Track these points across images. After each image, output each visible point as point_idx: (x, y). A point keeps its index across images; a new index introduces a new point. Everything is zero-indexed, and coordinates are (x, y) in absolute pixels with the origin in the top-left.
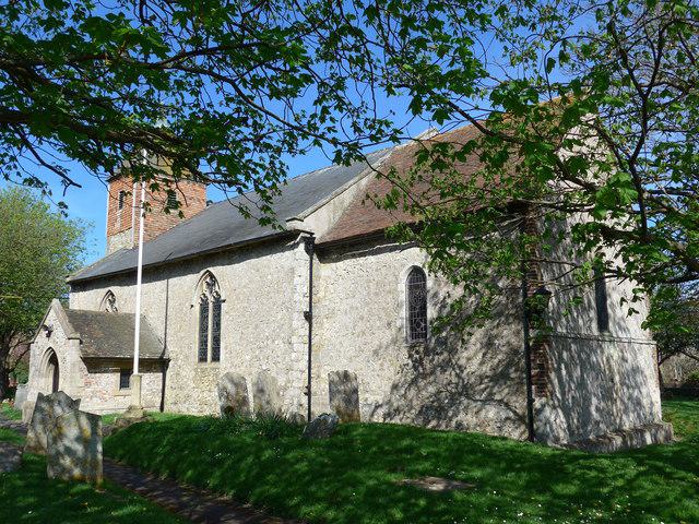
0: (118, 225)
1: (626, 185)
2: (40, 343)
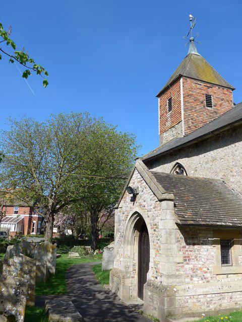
0: (168, 124)
1: (33, 245)
2: (124, 211)
